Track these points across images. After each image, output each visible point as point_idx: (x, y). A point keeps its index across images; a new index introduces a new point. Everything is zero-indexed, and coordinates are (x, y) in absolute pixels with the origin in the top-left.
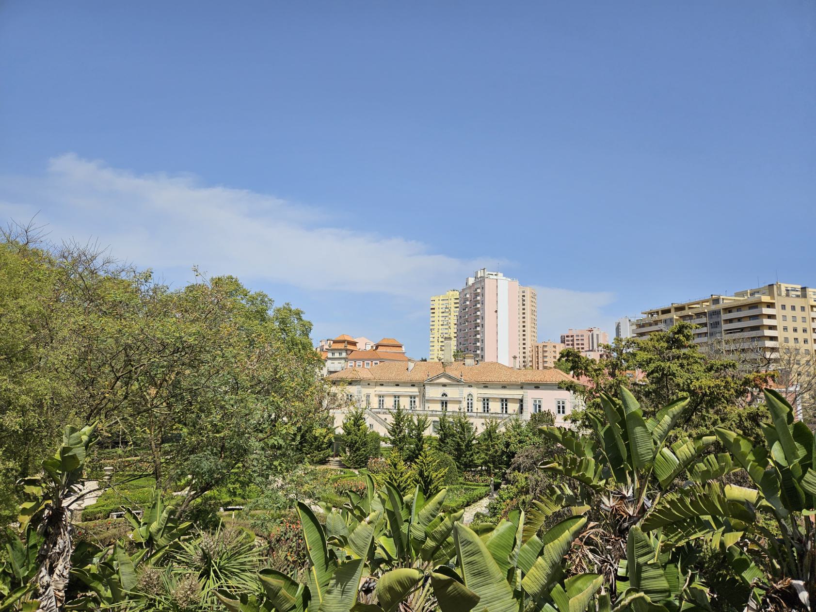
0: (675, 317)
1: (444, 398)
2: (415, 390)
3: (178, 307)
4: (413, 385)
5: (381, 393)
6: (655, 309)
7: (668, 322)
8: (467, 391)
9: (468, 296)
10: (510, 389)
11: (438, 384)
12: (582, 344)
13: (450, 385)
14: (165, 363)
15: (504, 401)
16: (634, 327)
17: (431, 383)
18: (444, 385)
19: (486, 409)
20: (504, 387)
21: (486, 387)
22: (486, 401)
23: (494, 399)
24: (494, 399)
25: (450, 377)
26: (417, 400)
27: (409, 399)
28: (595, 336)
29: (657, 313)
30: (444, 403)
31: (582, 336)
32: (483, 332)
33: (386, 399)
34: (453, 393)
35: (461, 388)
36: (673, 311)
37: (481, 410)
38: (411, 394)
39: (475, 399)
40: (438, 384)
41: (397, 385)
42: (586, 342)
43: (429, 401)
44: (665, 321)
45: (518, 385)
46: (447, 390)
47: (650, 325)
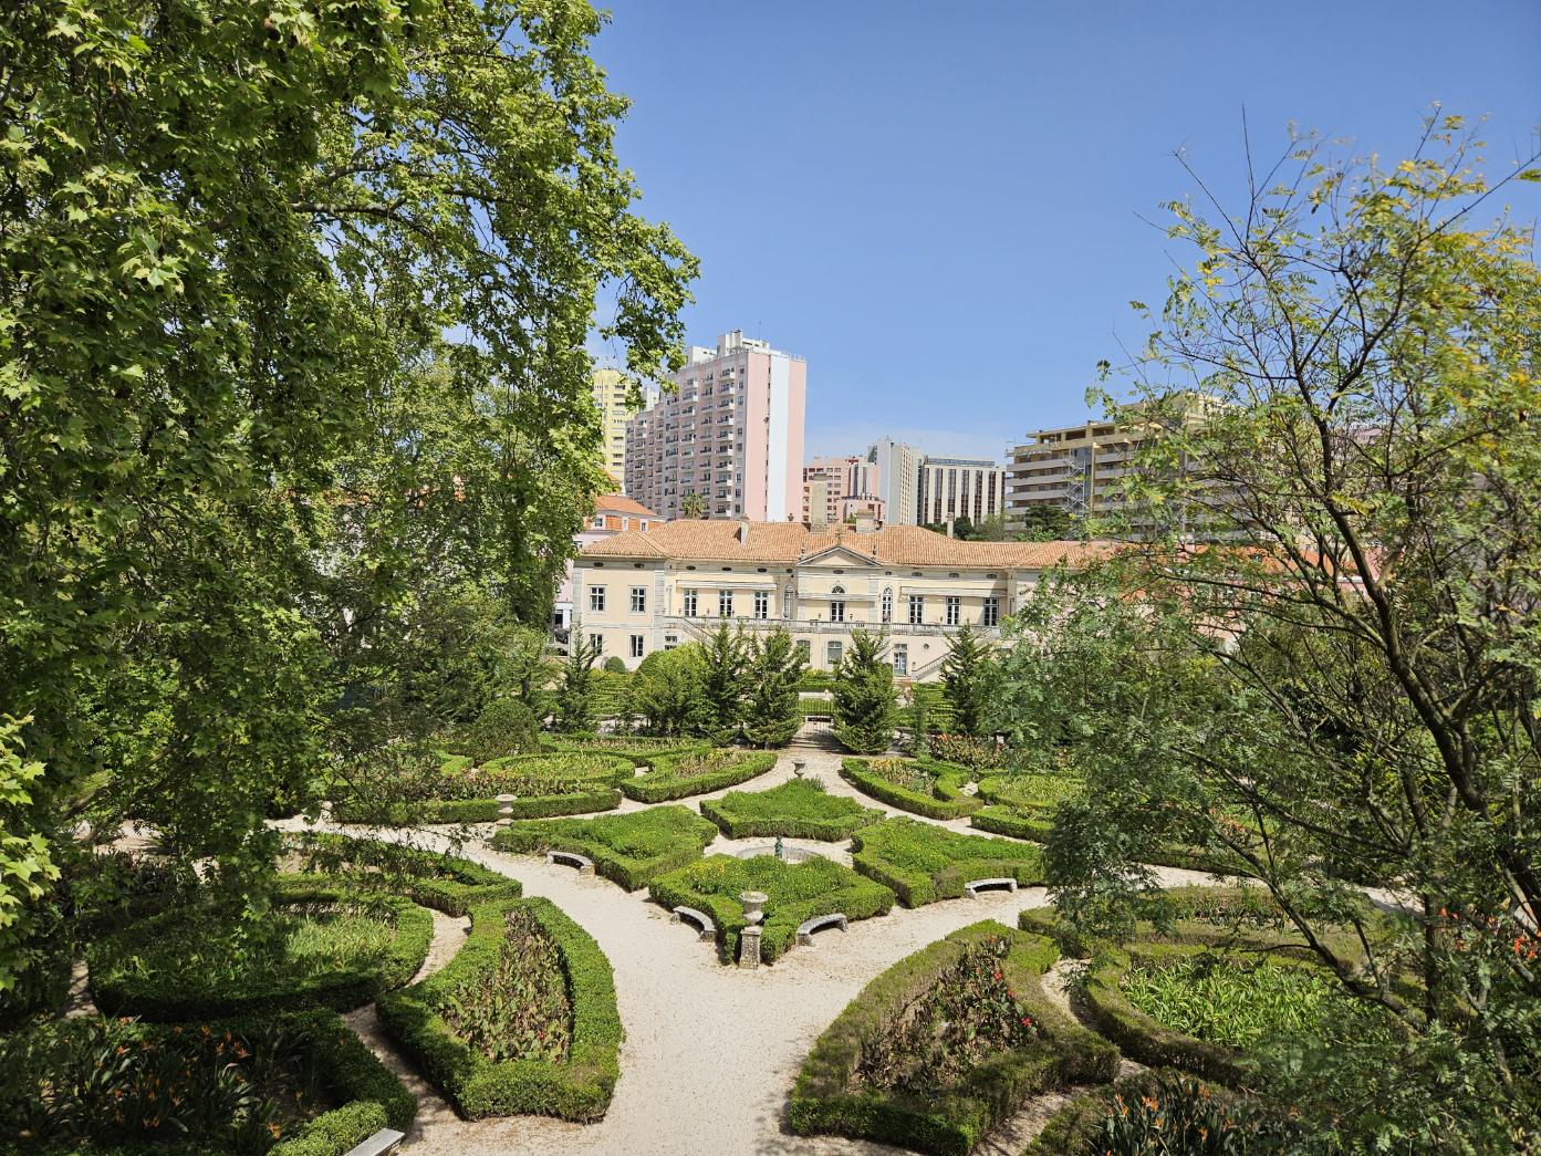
0: (1095, 446)
1: (838, 597)
2: (766, 581)
3: (406, 793)
4: (762, 570)
5: (691, 585)
6: (1047, 430)
7: (1081, 453)
8: (883, 582)
9: (696, 384)
10: (965, 579)
11: (824, 569)
12: (838, 485)
13: (852, 570)
14: (87, 87)
15: (953, 602)
16: (1011, 460)
17: (810, 566)
18: (839, 571)
19: (953, 616)
20: (954, 575)
21: (918, 575)
22: (916, 603)
23: (935, 598)
24: (935, 598)
25: (851, 555)
26: (771, 600)
27: (752, 598)
28: (860, 471)
29: (1059, 436)
30: (837, 608)
31: (838, 469)
32: (742, 461)
33: (701, 598)
34: (855, 585)
35: (873, 576)
36: (1089, 434)
37: (906, 618)
38: (757, 587)
39: (895, 597)
40: (824, 569)
41: (691, 568)
42: (844, 481)
43: (805, 602)
44: (1076, 452)
45: (982, 572)
46: (842, 580)
47: (1043, 457)
